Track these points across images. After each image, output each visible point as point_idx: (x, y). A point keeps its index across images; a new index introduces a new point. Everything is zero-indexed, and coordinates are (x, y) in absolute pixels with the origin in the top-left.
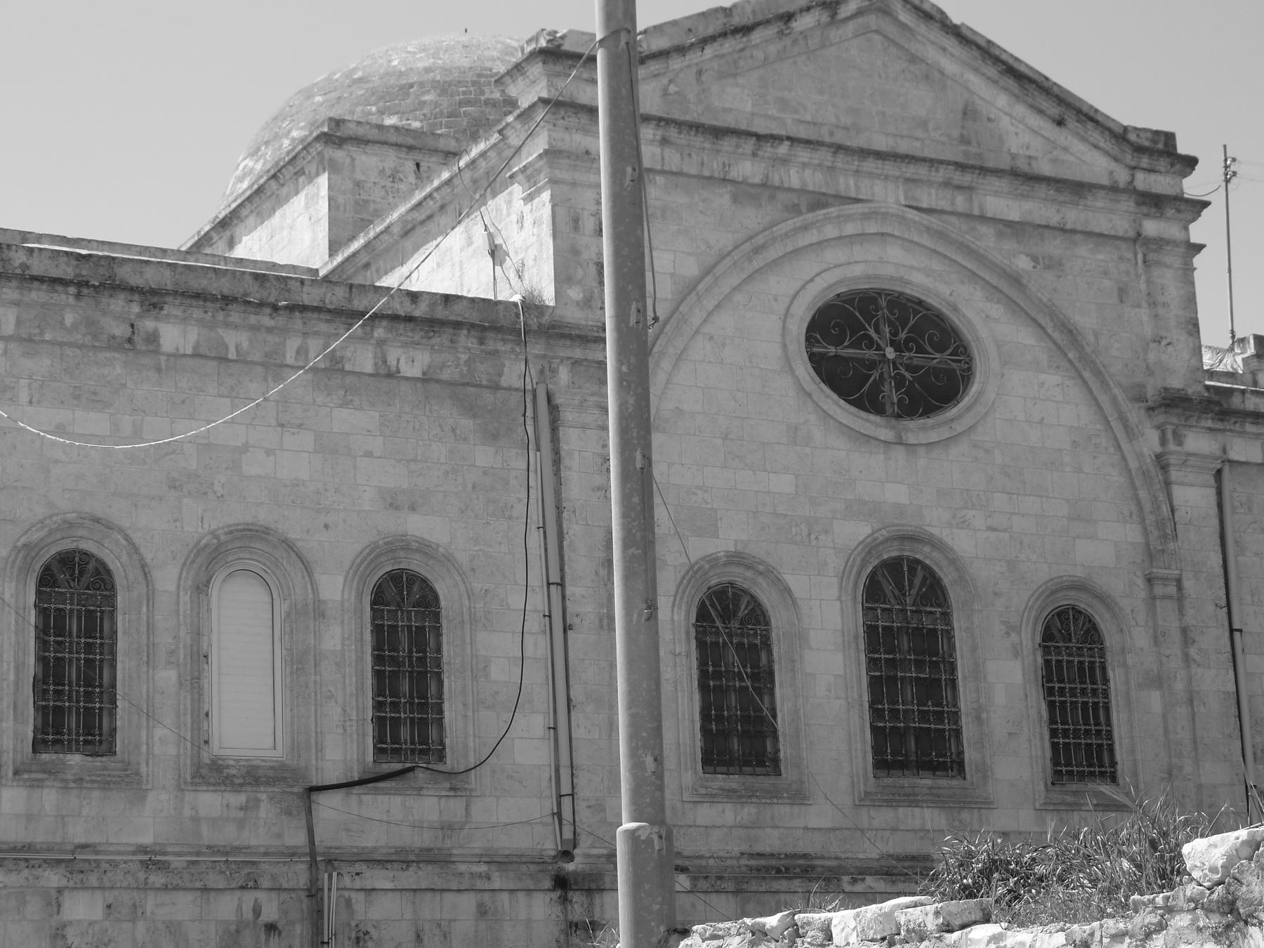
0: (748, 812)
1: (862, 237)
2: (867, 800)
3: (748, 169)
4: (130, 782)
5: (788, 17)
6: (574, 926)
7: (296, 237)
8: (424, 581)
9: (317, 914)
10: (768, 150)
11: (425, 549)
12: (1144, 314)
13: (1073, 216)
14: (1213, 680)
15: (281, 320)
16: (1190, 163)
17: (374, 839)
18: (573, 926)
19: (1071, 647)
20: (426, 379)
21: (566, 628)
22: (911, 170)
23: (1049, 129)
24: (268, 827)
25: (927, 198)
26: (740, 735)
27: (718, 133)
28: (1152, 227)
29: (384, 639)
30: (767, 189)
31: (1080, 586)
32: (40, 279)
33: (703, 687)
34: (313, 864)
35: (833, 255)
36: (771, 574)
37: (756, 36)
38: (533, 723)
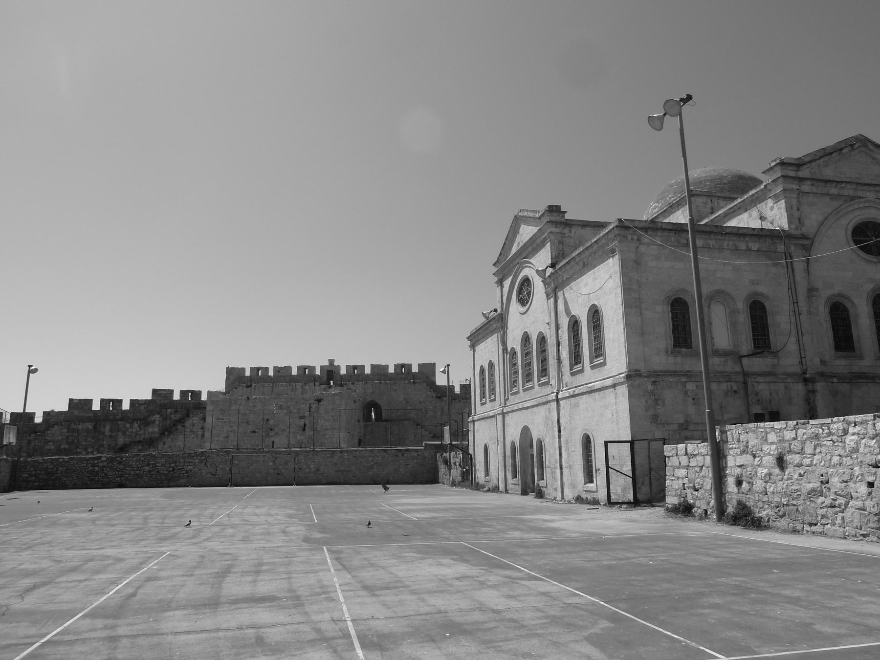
0: (848, 362)
3: (834, 191)
4: (861, 357)
5: (842, 149)
8: (762, 303)
10: (839, 186)
11: (762, 295)
17: (756, 369)
18: (809, 391)
20: (758, 251)
21: (800, 314)
24: (731, 366)
26: (844, 340)
29: (753, 318)
30: (839, 196)
32: (666, 229)
33: (833, 329)
34: (744, 376)
35: (857, 213)
36: (848, 298)
37: (833, 155)
38: (793, 339)
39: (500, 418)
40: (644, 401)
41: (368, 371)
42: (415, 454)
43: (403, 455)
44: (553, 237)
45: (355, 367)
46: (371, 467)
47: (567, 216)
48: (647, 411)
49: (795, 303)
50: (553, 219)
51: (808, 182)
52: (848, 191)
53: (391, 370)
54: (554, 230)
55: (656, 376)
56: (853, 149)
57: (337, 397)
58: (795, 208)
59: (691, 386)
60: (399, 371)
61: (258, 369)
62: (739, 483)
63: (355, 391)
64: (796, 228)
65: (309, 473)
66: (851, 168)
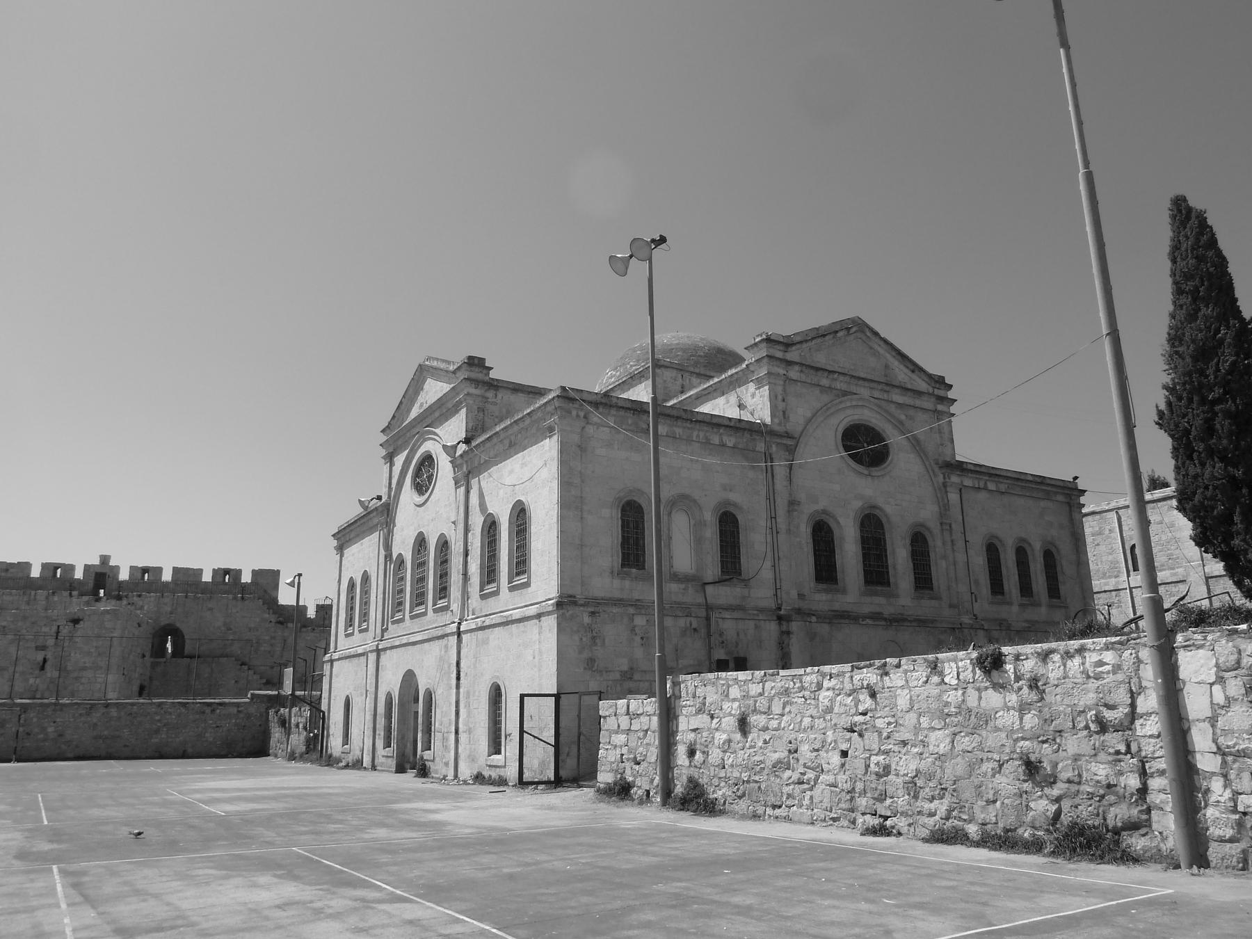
0: (829, 596)
3: (825, 382)
4: (844, 591)
5: (837, 332)
7: (642, 393)
9: (708, 626)
11: (735, 505)
13: (918, 403)
14: (961, 557)
16: (950, 387)
17: (722, 601)
18: (783, 633)
19: (919, 543)
22: (873, 385)
23: (910, 373)
24: (691, 596)
25: (877, 394)
27: (818, 369)
28: (940, 407)
29: (722, 533)
31: (922, 525)
35: (849, 412)
36: (834, 517)
38: (768, 564)
39: (372, 657)
40: (576, 638)
41: (167, 576)
42: (235, 710)
43: (213, 711)
45: (145, 570)
46: (157, 731)
47: (493, 375)
48: (580, 653)
49: (773, 518)
50: (473, 375)
51: (797, 368)
52: (840, 384)
53: (207, 577)
54: (473, 391)
56: (849, 334)
57: (108, 616)
58: (780, 398)
59: (640, 621)
60: (219, 579)
61: (56, 567)
62: (691, 753)
63: (142, 608)
64: (780, 424)
65: (45, 740)
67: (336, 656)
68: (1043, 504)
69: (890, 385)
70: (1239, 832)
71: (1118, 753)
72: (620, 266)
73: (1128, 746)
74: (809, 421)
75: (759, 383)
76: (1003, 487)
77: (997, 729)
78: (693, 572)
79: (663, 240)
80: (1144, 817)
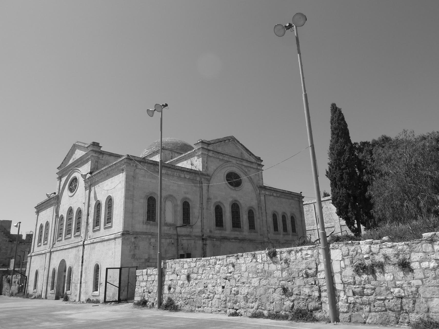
1: (231, 166)
2: (232, 231)
3: (221, 157)
4: (225, 230)
5: (225, 141)
6: (204, 244)
7: (157, 158)
9: (178, 242)
11: (189, 199)
12: (258, 177)
14: (264, 218)
15: (175, 170)
16: (262, 161)
17: (183, 233)
19: (251, 213)
22: (237, 159)
24: (172, 231)
25: (238, 162)
26: (219, 223)
27: (219, 153)
28: (259, 168)
31: (252, 207)
35: (229, 168)
38: (200, 220)
39: (48, 255)
40: (129, 247)
44: (93, 159)
47: (102, 149)
48: (130, 252)
50: (94, 149)
51: (212, 152)
54: (94, 155)
55: (136, 235)
58: (205, 162)
59: (153, 240)
62: (170, 288)
66: (228, 149)
67: (33, 254)
68: (291, 201)
69: (243, 159)
70: (348, 310)
71: (312, 284)
72: (151, 113)
73: (315, 282)
74: (215, 171)
75: (199, 157)
76: (278, 195)
77: (274, 277)
78: (173, 222)
79: (166, 105)
80: (320, 306)
